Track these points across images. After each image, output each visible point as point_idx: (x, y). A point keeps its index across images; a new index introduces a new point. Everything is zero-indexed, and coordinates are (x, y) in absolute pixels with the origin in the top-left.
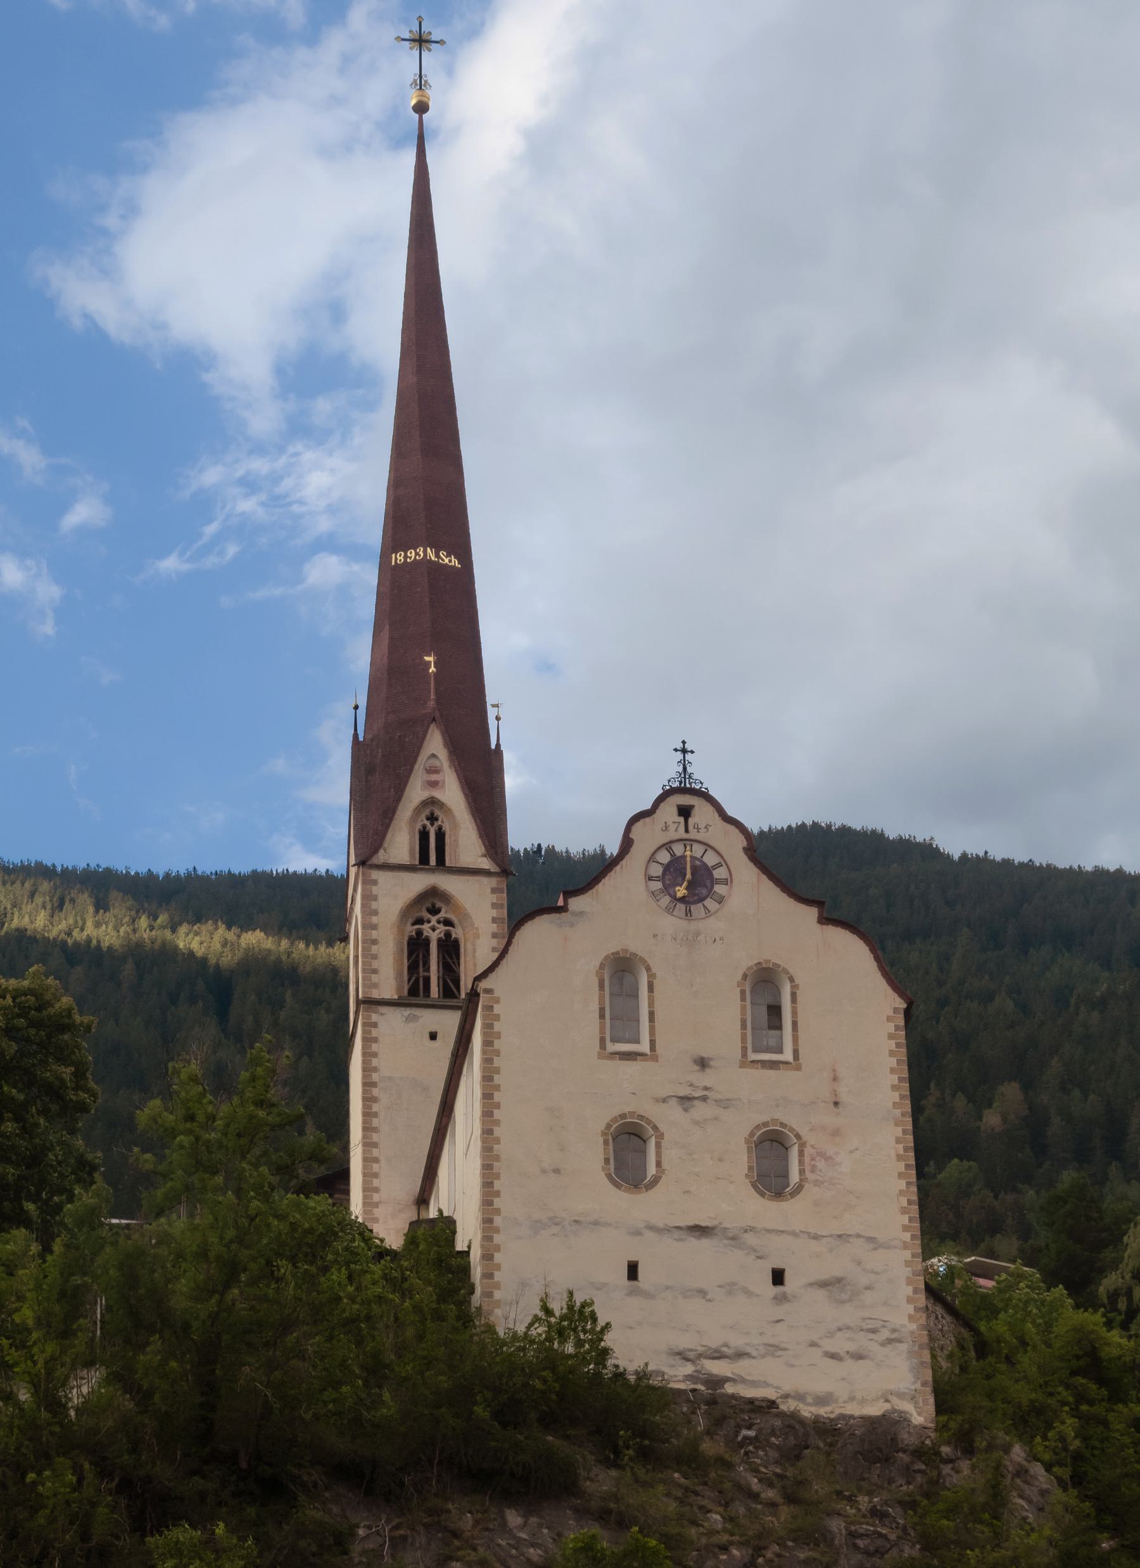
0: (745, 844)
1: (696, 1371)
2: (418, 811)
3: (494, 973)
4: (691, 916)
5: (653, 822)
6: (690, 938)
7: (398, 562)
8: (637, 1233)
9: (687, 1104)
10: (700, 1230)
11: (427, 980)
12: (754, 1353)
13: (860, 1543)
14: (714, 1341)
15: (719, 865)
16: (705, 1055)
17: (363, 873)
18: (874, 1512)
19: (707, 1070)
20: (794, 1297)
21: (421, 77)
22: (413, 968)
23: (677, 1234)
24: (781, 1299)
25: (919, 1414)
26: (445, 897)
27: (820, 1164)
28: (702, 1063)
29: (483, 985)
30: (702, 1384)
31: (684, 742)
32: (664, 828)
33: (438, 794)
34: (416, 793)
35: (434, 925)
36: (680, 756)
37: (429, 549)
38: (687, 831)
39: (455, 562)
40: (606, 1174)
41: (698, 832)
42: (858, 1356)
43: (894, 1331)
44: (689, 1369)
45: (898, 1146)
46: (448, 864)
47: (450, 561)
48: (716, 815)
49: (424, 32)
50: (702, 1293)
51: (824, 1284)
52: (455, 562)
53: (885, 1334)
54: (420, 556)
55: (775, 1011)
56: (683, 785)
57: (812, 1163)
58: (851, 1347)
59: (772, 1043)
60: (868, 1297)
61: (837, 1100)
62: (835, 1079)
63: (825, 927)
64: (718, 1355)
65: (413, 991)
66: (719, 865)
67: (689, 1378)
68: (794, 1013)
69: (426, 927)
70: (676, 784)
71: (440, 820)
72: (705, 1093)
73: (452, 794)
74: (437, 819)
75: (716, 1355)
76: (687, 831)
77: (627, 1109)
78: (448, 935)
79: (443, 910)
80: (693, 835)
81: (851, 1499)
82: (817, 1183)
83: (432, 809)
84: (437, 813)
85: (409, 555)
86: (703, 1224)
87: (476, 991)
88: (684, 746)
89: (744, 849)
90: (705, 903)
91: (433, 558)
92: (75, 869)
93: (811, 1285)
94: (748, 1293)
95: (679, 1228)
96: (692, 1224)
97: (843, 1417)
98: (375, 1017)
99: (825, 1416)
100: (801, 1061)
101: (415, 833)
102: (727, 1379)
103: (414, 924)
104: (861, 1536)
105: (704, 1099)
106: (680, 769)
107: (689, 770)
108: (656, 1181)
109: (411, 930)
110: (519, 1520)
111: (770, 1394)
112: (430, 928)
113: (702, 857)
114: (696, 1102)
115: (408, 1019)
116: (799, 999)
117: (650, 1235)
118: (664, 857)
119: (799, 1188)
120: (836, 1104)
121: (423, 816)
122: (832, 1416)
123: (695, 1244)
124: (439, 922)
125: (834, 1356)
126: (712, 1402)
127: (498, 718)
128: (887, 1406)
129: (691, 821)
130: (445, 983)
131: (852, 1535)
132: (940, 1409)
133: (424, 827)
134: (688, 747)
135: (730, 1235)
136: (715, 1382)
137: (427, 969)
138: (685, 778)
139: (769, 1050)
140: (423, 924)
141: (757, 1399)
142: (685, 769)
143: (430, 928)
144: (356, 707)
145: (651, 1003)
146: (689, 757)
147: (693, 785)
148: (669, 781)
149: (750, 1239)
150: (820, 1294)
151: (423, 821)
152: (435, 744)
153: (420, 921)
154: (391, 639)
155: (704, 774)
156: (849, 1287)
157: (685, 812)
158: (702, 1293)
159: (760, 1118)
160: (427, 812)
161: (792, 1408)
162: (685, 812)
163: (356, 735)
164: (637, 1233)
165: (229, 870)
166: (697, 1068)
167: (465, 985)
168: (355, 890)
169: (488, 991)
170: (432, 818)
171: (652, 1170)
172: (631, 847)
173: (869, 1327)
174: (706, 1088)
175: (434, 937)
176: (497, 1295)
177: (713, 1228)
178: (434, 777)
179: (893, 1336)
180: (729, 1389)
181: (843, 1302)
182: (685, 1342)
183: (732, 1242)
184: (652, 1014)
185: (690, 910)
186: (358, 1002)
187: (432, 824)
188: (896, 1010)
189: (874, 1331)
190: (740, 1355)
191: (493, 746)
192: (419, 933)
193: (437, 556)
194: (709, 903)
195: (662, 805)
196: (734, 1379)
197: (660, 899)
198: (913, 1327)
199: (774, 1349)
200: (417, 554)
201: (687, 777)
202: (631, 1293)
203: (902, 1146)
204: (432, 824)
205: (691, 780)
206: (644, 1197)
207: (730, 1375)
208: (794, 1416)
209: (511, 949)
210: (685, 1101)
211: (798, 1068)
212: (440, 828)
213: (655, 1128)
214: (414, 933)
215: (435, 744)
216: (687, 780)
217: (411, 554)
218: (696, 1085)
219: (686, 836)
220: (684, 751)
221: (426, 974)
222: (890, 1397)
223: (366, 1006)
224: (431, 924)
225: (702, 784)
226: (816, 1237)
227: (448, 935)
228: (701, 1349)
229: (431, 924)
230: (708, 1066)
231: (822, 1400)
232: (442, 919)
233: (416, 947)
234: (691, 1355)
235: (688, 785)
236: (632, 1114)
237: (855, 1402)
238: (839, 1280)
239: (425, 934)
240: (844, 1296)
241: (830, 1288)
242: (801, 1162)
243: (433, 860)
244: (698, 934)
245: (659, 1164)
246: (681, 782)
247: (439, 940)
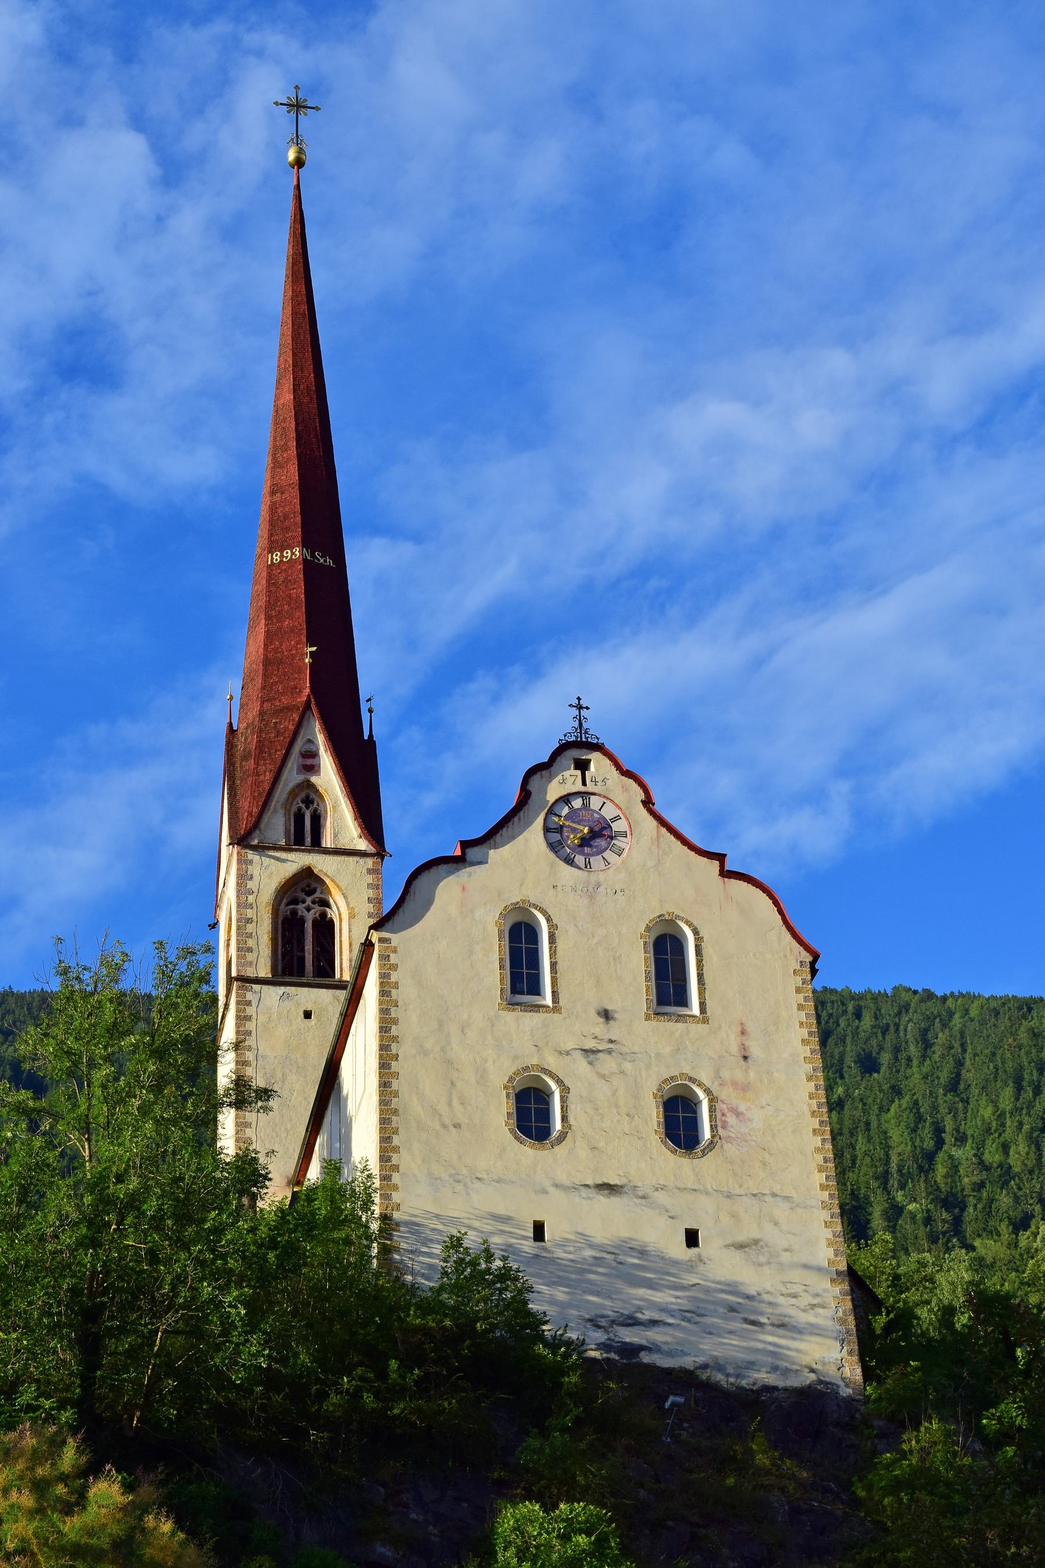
0: (643, 797)
1: (609, 1339)
2: (293, 793)
3: (391, 922)
4: (591, 868)
5: (550, 775)
6: (591, 889)
7: (279, 554)
9: (592, 1057)
11: (302, 960)
15: (617, 818)
16: (609, 1008)
17: (238, 853)
19: (611, 1022)
20: (721, 1248)
21: (297, 136)
23: (584, 1192)
27: (731, 1119)
30: (615, 1353)
31: (579, 699)
32: (561, 781)
35: (309, 905)
36: (576, 712)
38: (584, 783)
39: (329, 562)
40: (509, 1129)
41: (596, 785)
43: (817, 1295)
44: (600, 1336)
45: (810, 1101)
47: (325, 561)
48: (613, 769)
49: (301, 99)
51: (740, 1246)
52: (329, 562)
54: (296, 555)
56: (579, 739)
57: (723, 1118)
61: (747, 1054)
62: (743, 1033)
63: (726, 879)
64: (631, 1322)
66: (617, 818)
69: (301, 907)
70: (573, 739)
71: (316, 803)
72: (611, 1046)
74: (312, 802)
75: (629, 1321)
76: (584, 783)
78: (324, 915)
80: (590, 787)
85: (285, 555)
86: (612, 1183)
87: (371, 941)
88: (579, 702)
90: (604, 855)
91: (309, 558)
96: (600, 1182)
99: (748, 1387)
100: (709, 1014)
101: (290, 815)
102: (642, 1348)
105: (609, 1052)
106: (576, 724)
107: (585, 725)
108: (562, 1137)
112: (305, 908)
113: (600, 810)
114: (600, 1055)
116: (704, 952)
120: (745, 1058)
121: (299, 799)
122: (755, 1388)
123: (603, 1201)
124: (314, 902)
127: (370, 711)
133: (300, 809)
134: (584, 703)
135: (640, 1194)
136: (631, 1350)
138: (581, 733)
140: (297, 904)
142: (581, 724)
143: (305, 908)
146: (584, 712)
147: (589, 740)
148: (565, 736)
149: (660, 1197)
153: (295, 901)
154: (267, 632)
156: (766, 1249)
157: (583, 766)
160: (303, 795)
161: (718, 1379)
165: (42, 989)
166: (602, 1020)
168: (227, 872)
170: (308, 801)
171: (558, 1125)
172: (529, 799)
173: (789, 1291)
174: (611, 1041)
175: (310, 917)
177: (622, 1187)
178: (309, 762)
179: (815, 1302)
180: (646, 1358)
181: (760, 1265)
183: (643, 1201)
185: (589, 862)
186: (230, 980)
187: (307, 807)
191: (366, 738)
192: (294, 913)
194: (608, 854)
195: (559, 758)
196: (648, 1347)
197: (559, 850)
200: (293, 554)
201: (583, 732)
203: (815, 1101)
204: (307, 807)
205: (587, 736)
207: (644, 1342)
209: (408, 898)
212: (316, 810)
214: (288, 913)
216: (583, 735)
218: (600, 1038)
219: (583, 789)
220: (580, 708)
221: (299, 954)
223: (239, 983)
224: (306, 904)
225: (598, 739)
229: (306, 904)
230: (613, 1018)
232: (317, 899)
234: (603, 1322)
235: (584, 740)
237: (778, 1372)
238: (756, 1242)
239: (300, 913)
240: (762, 1259)
241: (747, 1249)
243: (308, 840)
244: (598, 885)
245: (564, 1118)
246: (577, 737)
247: (315, 923)
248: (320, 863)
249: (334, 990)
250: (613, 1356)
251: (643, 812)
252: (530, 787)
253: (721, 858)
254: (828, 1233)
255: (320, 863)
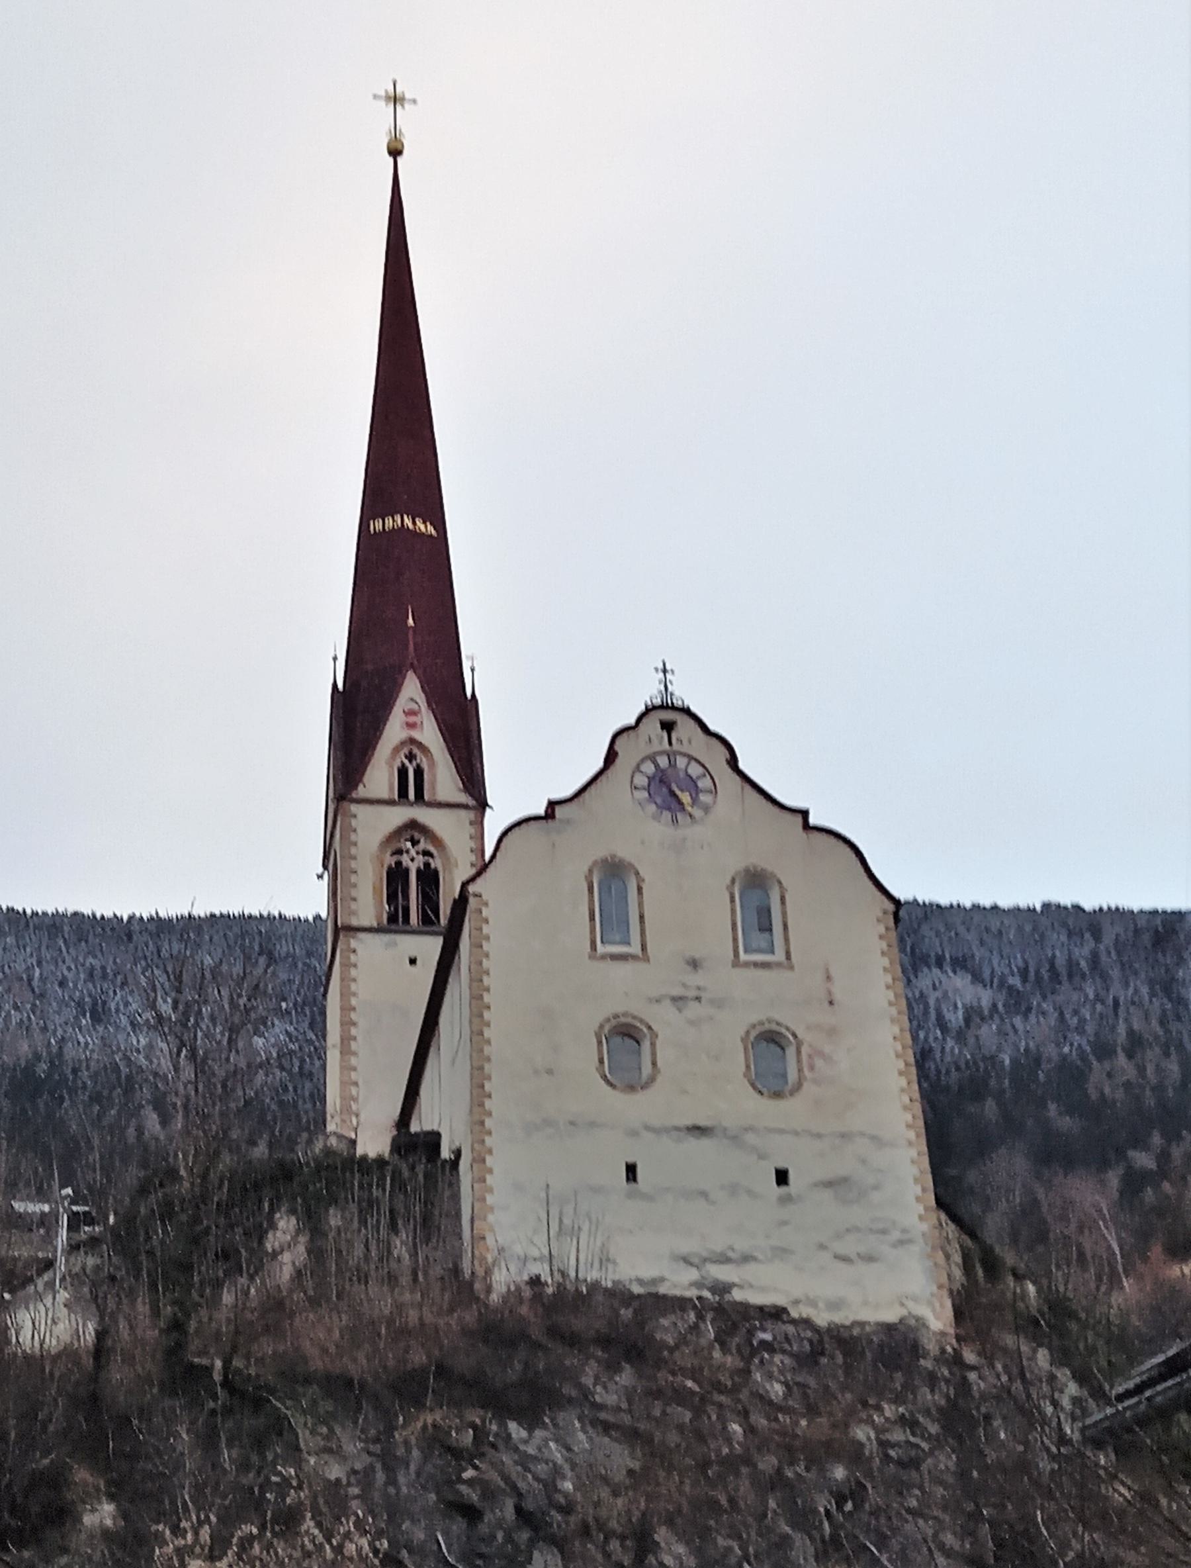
2: (396, 750)
8: (634, 1133)
9: (680, 1003)
10: (698, 1130)
11: (406, 910)
12: (760, 1257)
13: (892, 1453)
14: (718, 1244)
16: (697, 956)
18: (902, 1420)
22: (391, 898)
23: (675, 1134)
24: (786, 1200)
25: (937, 1318)
26: (424, 830)
27: (819, 1063)
28: (694, 964)
29: (472, 888)
33: (416, 735)
34: (394, 731)
37: (405, 517)
38: (670, 743)
39: (431, 530)
42: (870, 1259)
44: (693, 1275)
46: (426, 797)
50: (704, 1194)
51: (829, 1184)
53: (896, 1235)
55: (764, 915)
58: (862, 1249)
59: (764, 945)
60: (876, 1197)
64: (723, 1259)
65: (392, 918)
67: (698, 1285)
68: (784, 914)
71: (418, 758)
73: (430, 734)
76: (670, 743)
77: (620, 1009)
78: (427, 865)
79: (422, 840)
81: (878, 1408)
82: (816, 1082)
83: (412, 748)
84: (416, 751)
89: (727, 760)
92: (45, 914)
93: (816, 1185)
94: (750, 1193)
95: (677, 1129)
97: (855, 1323)
98: (353, 944)
102: (734, 1285)
103: (393, 854)
104: (893, 1446)
105: (698, 999)
106: (662, 688)
109: (390, 860)
110: (524, 1434)
111: (779, 1300)
115: (388, 945)
117: (648, 1136)
118: (649, 768)
119: (799, 1086)
120: (831, 1003)
123: (694, 1144)
125: (845, 1259)
126: (720, 1310)
128: (904, 1312)
129: (674, 736)
130: (424, 910)
131: (884, 1444)
132: (959, 1314)
136: (722, 1289)
137: (406, 897)
139: (759, 951)
141: (766, 1306)
144: (335, 659)
145: (641, 905)
149: (750, 1138)
150: (827, 1194)
151: (402, 758)
152: (411, 690)
153: (399, 852)
155: (684, 694)
158: (704, 1194)
159: (754, 1018)
160: (406, 750)
162: (668, 727)
163: (335, 685)
164: (634, 1133)
167: (445, 912)
169: (477, 895)
170: (411, 757)
174: (699, 988)
176: (490, 1199)
178: (412, 719)
180: (737, 1295)
182: (687, 1246)
184: (642, 917)
188: (885, 912)
189: (884, 1232)
190: (747, 1258)
192: (399, 863)
193: (414, 523)
198: (925, 1227)
199: (781, 1253)
202: (630, 1196)
204: (410, 761)
206: (640, 1097)
207: (736, 1280)
208: (807, 1322)
210: (678, 1001)
211: (791, 968)
213: (650, 1028)
215: (411, 690)
217: (389, 522)
222: (904, 1301)
226: (819, 1136)
227: (427, 865)
228: (705, 1254)
231: (835, 1305)
233: (396, 877)
234: (696, 1260)
236: (625, 1014)
242: (799, 1061)
244: (684, 839)
245: (654, 1064)
247: (419, 871)
248: (424, 815)
249: (922, 1117)
250: (707, 1294)
251: (729, 770)
252: (617, 748)
253: (805, 814)
254: (915, 1171)
255: (424, 815)
